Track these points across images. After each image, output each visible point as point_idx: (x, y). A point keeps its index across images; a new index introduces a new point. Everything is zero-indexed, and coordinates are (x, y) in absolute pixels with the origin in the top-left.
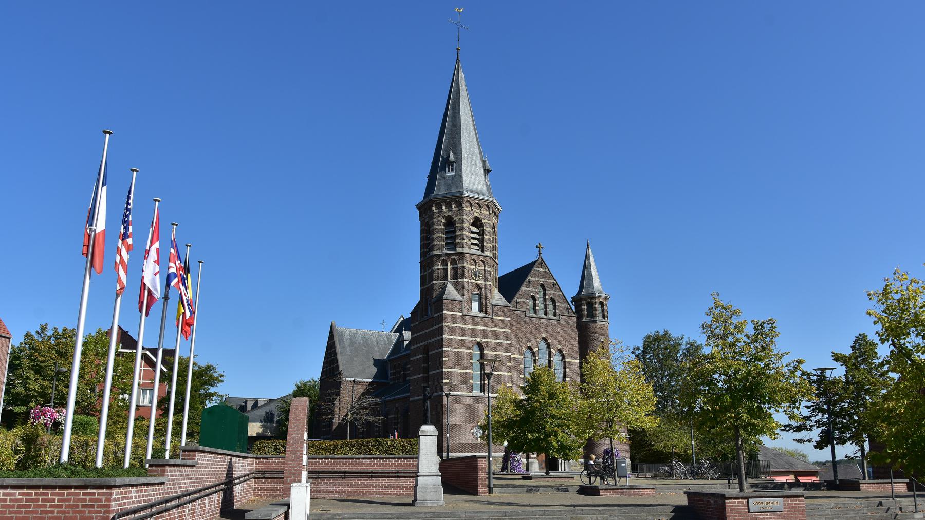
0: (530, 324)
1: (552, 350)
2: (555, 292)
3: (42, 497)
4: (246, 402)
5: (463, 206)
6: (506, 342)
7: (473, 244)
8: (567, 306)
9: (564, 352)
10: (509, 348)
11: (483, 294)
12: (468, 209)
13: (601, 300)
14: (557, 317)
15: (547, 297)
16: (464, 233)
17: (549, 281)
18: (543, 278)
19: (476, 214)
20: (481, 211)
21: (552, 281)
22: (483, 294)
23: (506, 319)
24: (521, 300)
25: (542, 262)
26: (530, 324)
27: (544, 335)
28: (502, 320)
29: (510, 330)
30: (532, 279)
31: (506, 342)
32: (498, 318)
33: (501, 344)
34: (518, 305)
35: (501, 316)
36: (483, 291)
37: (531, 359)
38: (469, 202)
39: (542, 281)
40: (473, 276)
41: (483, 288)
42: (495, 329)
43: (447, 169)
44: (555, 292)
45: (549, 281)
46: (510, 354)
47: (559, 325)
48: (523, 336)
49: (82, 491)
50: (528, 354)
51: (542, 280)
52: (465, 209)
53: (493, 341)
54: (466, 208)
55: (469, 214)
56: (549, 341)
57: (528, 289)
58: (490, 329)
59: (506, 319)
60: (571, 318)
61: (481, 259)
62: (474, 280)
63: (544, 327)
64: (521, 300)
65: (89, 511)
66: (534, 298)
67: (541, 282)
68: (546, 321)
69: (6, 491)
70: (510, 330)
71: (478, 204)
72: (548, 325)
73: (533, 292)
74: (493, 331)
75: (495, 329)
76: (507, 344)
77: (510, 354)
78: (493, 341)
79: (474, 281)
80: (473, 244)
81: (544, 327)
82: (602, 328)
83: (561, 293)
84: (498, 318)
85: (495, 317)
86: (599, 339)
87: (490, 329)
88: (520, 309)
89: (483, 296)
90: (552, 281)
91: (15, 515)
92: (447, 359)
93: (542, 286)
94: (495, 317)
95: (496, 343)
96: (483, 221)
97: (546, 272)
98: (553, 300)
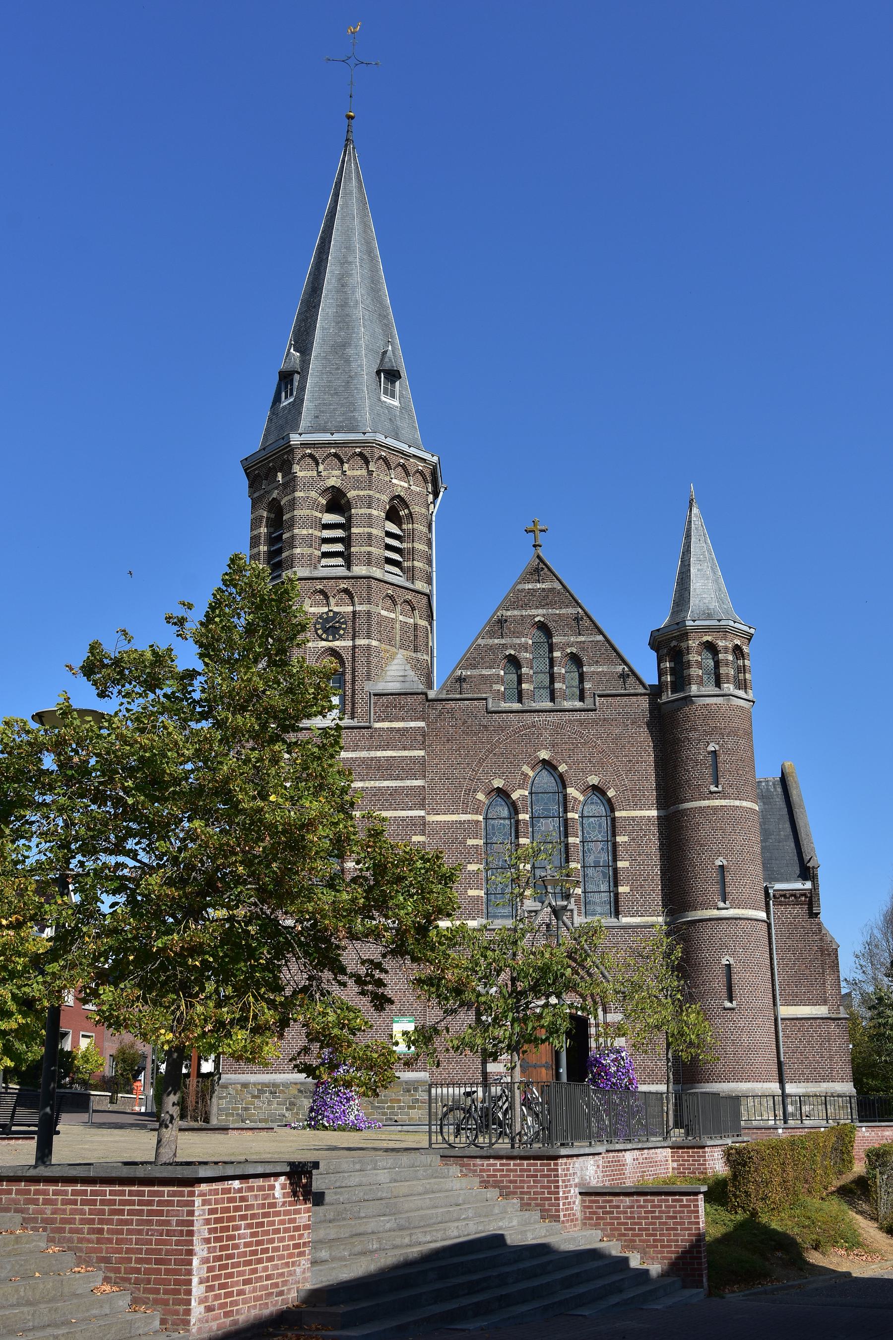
0: (501, 729)
1: (570, 790)
2: (582, 639)
3: (124, 1198)
4: (419, 982)
5: (296, 468)
6: (408, 783)
7: (326, 555)
8: (620, 669)
9: (611, 793)
10: (420, 799)
11: (349, 670)
12: (310, 473)
13: (707, 638)
14: (588, 703)
15: (557, 654)
16: (296, 531)
17: (563, 611)
18: (542, 607)
19: (332, 482)
20: (344, 472)
21: (571, 611)
22: (349, 670)
23: (413, 724)
24: (476, 672)
25: (541, 565)
26: (501, 729)
27: (544, 755)
28: (398, 730)
29: (422, 753)
30: (509, 613)
31: (408, 783)
32: (386, 725)
33: (396, 789)
34: (464, 686)
35: (397, 719)
36: (348, 665)
37: (507, 822)
38: (311, 456)
39: (539, 614)
40: (320, 632)
41: (347, 656)
42: (379, 754)
43: (283, 394)
44: (582, 639)
45: (563, 611)
46: (422, 813)
47: (595, 722)
48: (480, 762)
49: (89, 1189)
50: (499, 808)
51: (540, 611)
52: (300, 474)
53: (372, 784)
54: (301, 472)
55: (310, 485)
56: (562, 768)
57: (496, 641)
58: (364, 754)
59: (413, 724)
60: (634, 699)
61: (342, 586)
62: (323, 640)
63: (546, 734)
64: (476, 672)
65: (674, 1222)
66: (514, 662)
67: (537, 619)
68: (553, 718)
69: (38, 1187)
70: (422, 753)
71: (336, 455)
72: (558, 728)
73: (513, 646)
74: (372, 759)
75: (379, 754)
76: (412, 788)
77: (422, 813)
78: (372, 784)
79: (324, 644)
80: (326, 555)
81: (546, 734)
82: (710, 713)
83: (600, 638)
84: (386, 725)
85: (378, 725)
86: (701, 745)
87: (364, 754)
88: (470, 696)
89: (348, 677)
90: (571, 611)
91: (186, 1228)
92: (626, 839)
93: (543, 628)
94: (378, 725)
95: (379, 789)
96: (351, 494)
97: (552, 590)
98: (576, 660)
